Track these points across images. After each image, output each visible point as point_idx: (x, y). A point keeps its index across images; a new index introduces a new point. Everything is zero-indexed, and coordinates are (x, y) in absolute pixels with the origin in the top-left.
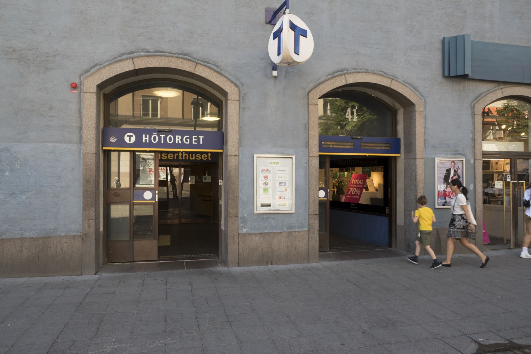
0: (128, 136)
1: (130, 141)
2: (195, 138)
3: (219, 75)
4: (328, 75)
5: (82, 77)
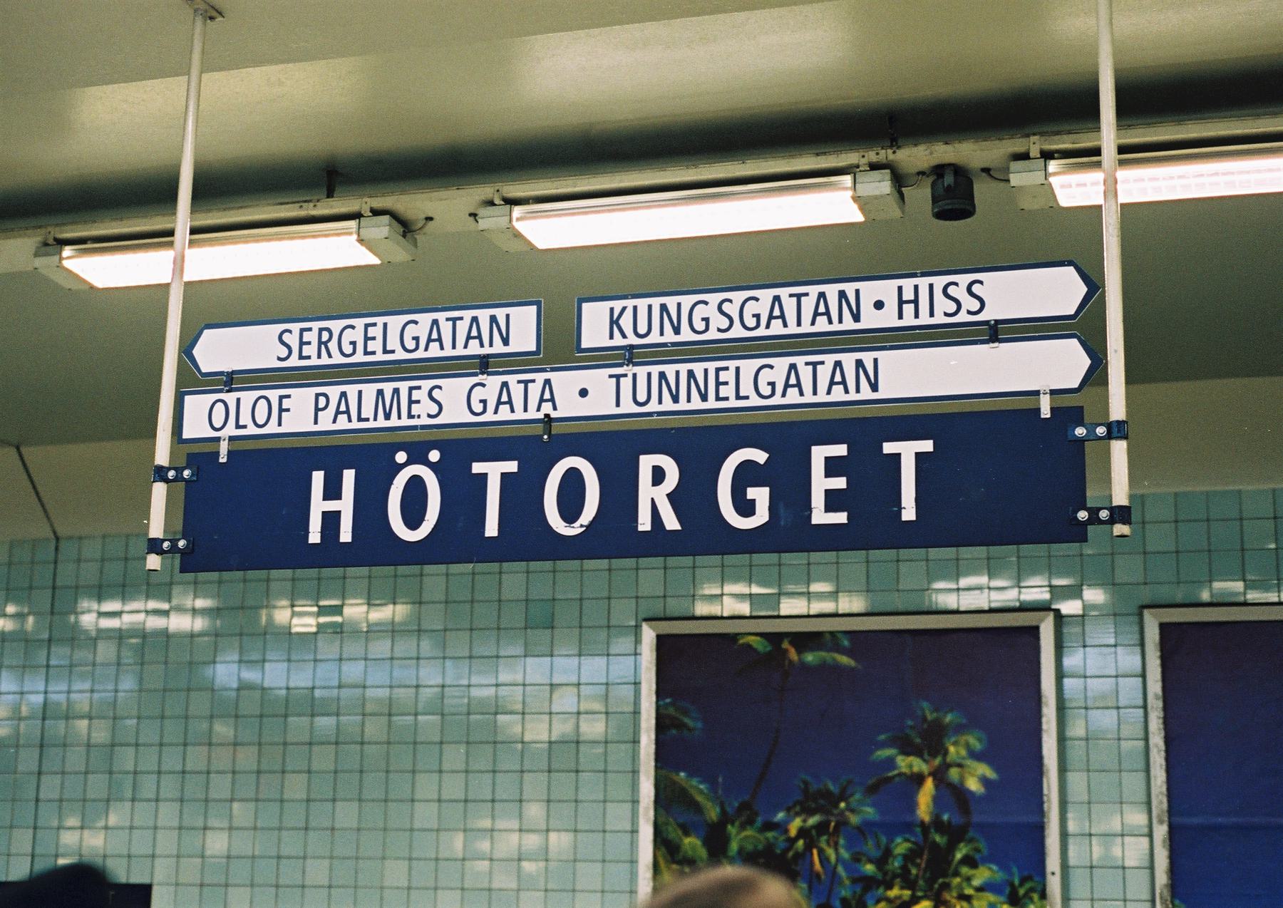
2: (833, 466)
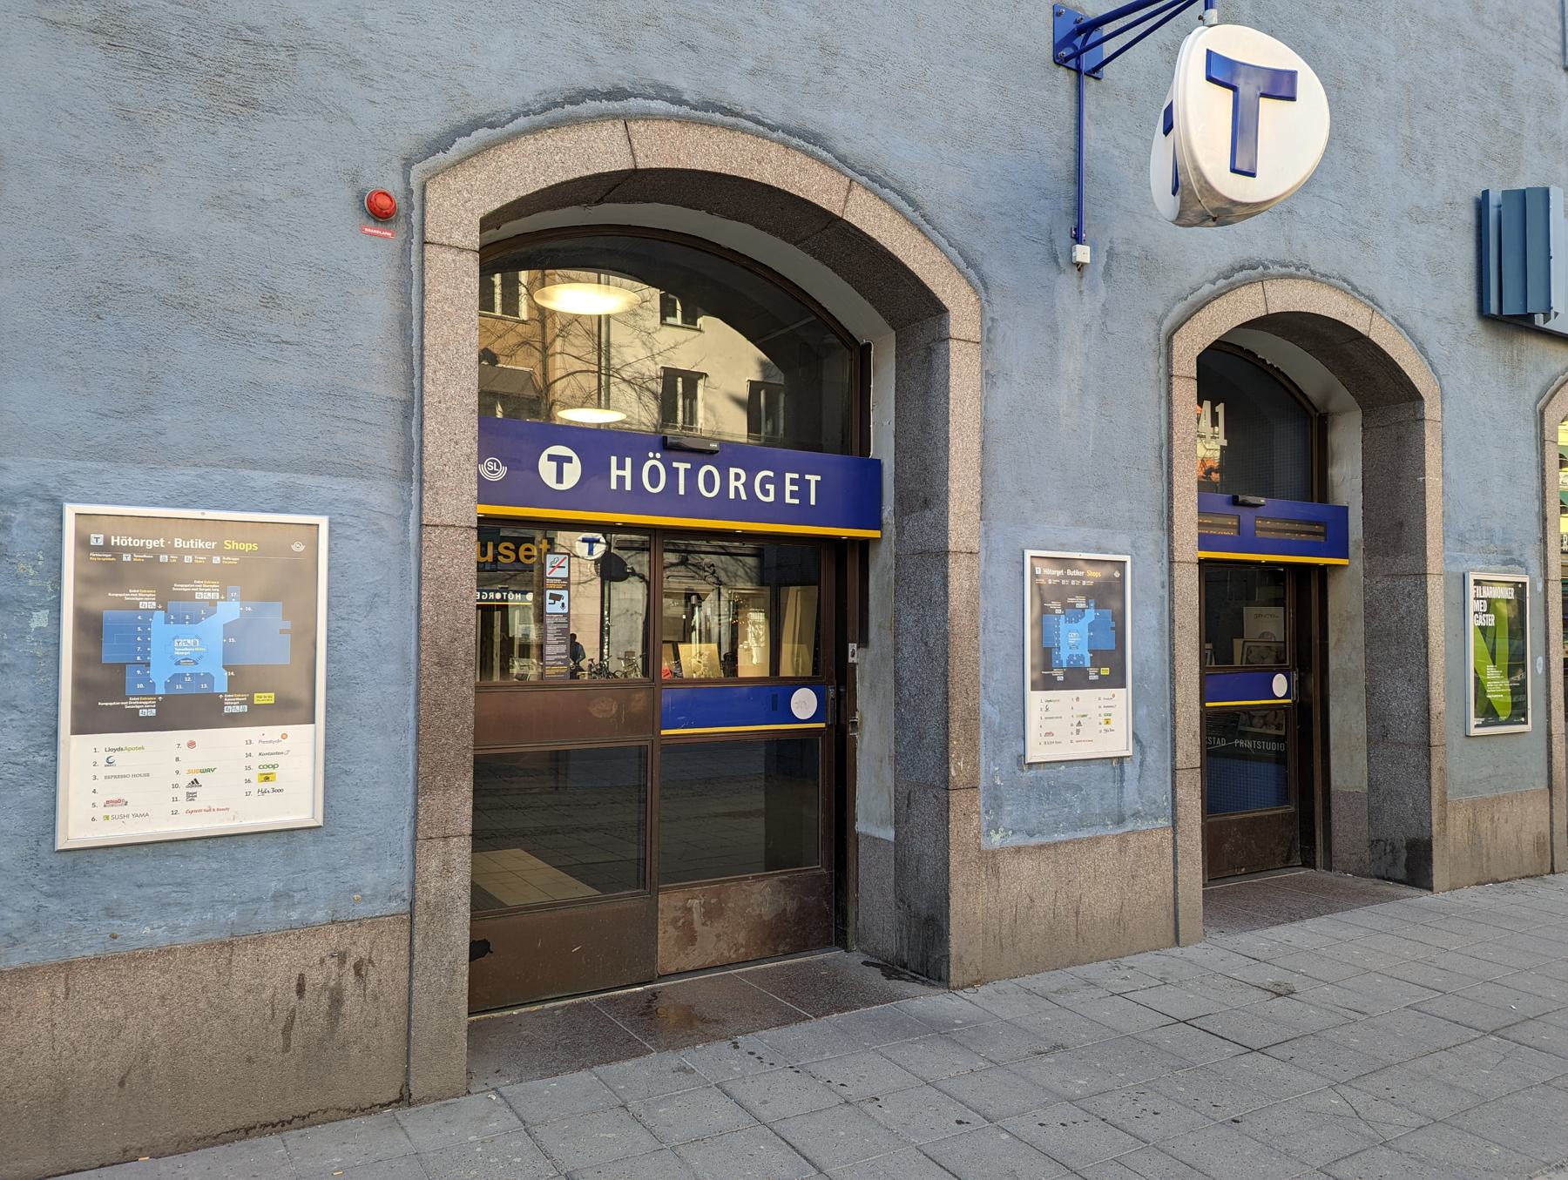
0: (551, 458)
1: (560, 479)
2: (793, 482)
3: (920, 237)
4: (1218, 278)
5: (416, 172)
